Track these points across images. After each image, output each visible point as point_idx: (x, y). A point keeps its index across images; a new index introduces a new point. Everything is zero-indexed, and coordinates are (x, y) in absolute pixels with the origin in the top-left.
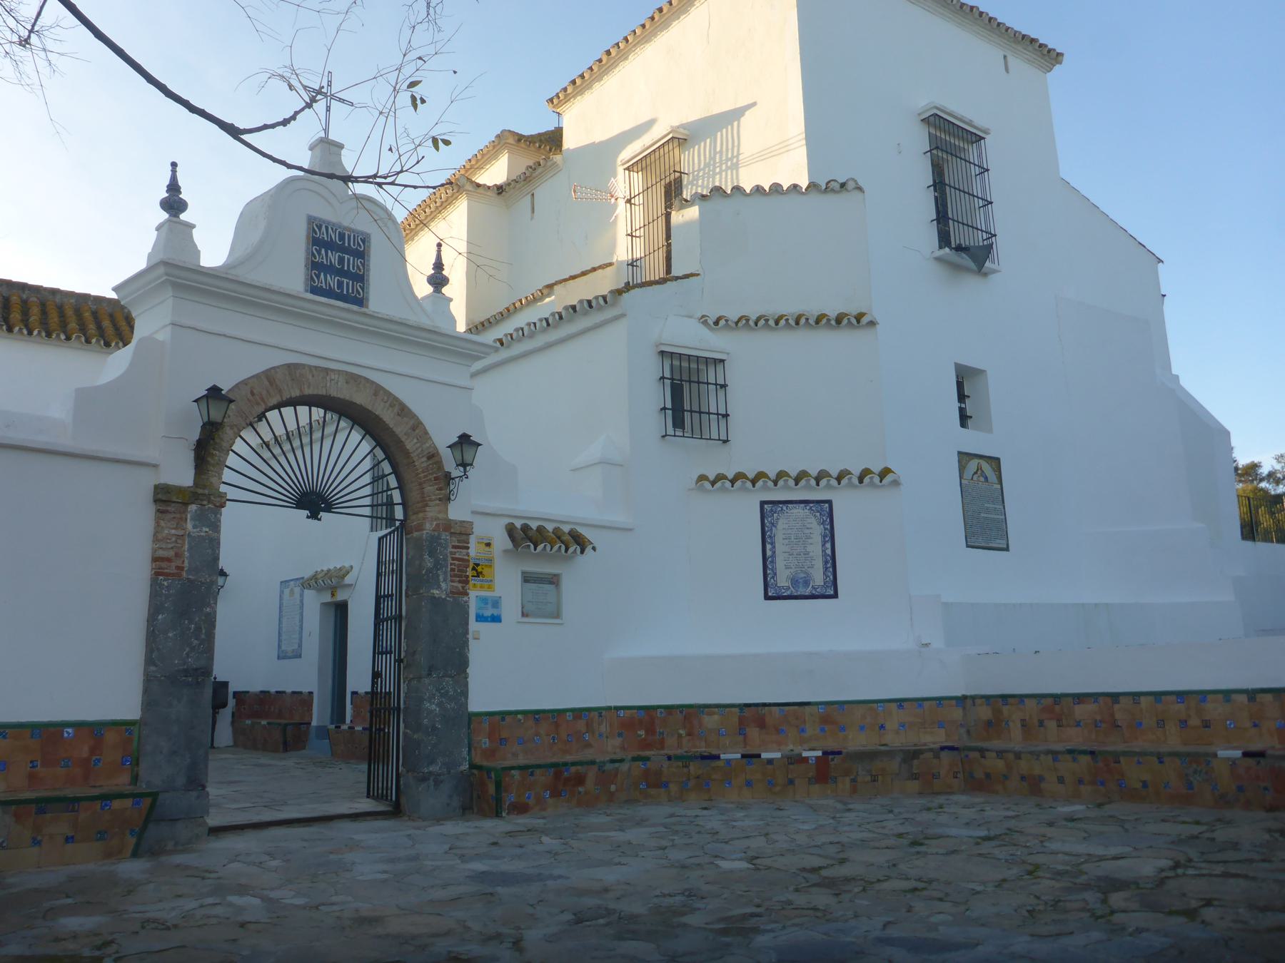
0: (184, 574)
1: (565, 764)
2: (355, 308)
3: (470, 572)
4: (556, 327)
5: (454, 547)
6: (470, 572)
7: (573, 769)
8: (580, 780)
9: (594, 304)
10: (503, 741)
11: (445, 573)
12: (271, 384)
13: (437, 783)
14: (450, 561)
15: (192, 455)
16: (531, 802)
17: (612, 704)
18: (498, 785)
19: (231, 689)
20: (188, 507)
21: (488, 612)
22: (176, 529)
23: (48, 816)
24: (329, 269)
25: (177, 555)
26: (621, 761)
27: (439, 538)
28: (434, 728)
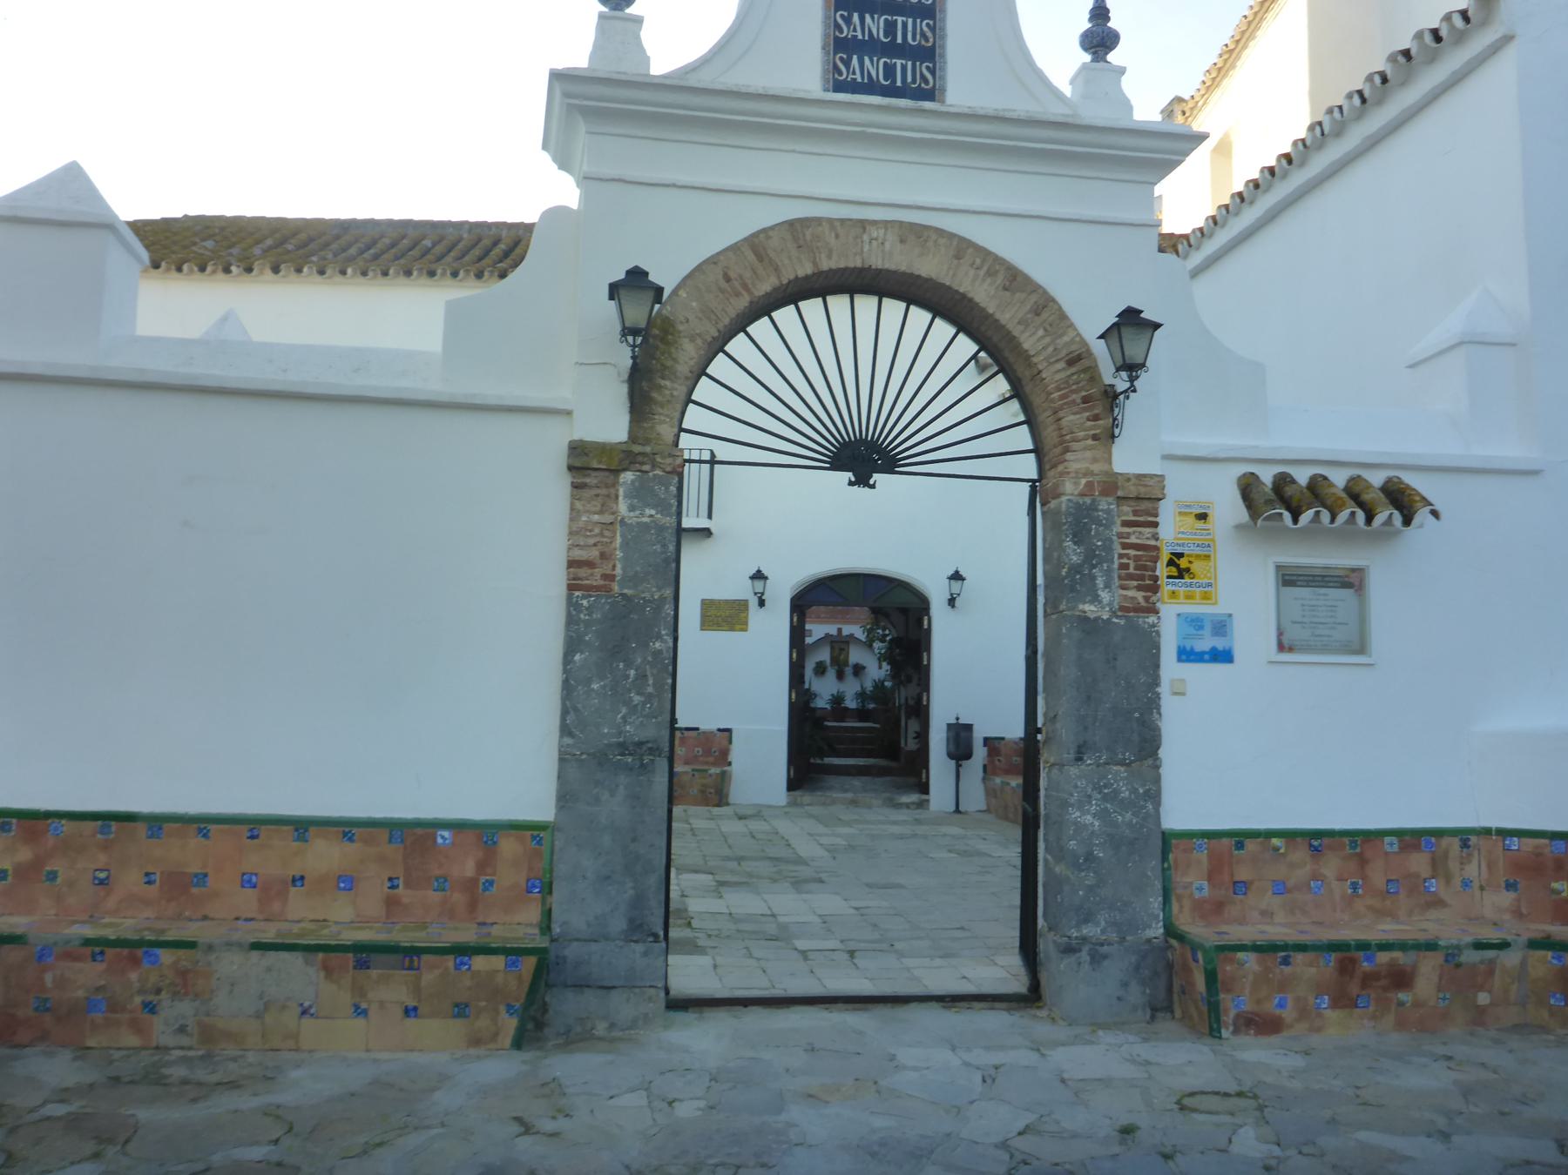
0: (616, 588)
1: (1363, 946)
2: (927, 105)
3: (1162, 570)
4: (1380, 102)
5: (1126, 524)
6: (1162, 570)
7: (1383, 957)
8: (1401, 979)
9: (1444, 33)
10: (1240, 887)
11: (1108, 573)
12: (760, 258)
13: (1097, 959)
14: (1118, 550)
15: (625, 389)
16: (1288, 1014)
17: (1494, 823)
18: (1211, 977)
19: (979, 735)
20: (632, 483)
21: (1205, 643)
22: (601, 512)
23: (374, 973)
24: (869, 47)
25: (603, 555)
26: (1504, 945)
27: (1093, 507)
28: (1090, 857)
